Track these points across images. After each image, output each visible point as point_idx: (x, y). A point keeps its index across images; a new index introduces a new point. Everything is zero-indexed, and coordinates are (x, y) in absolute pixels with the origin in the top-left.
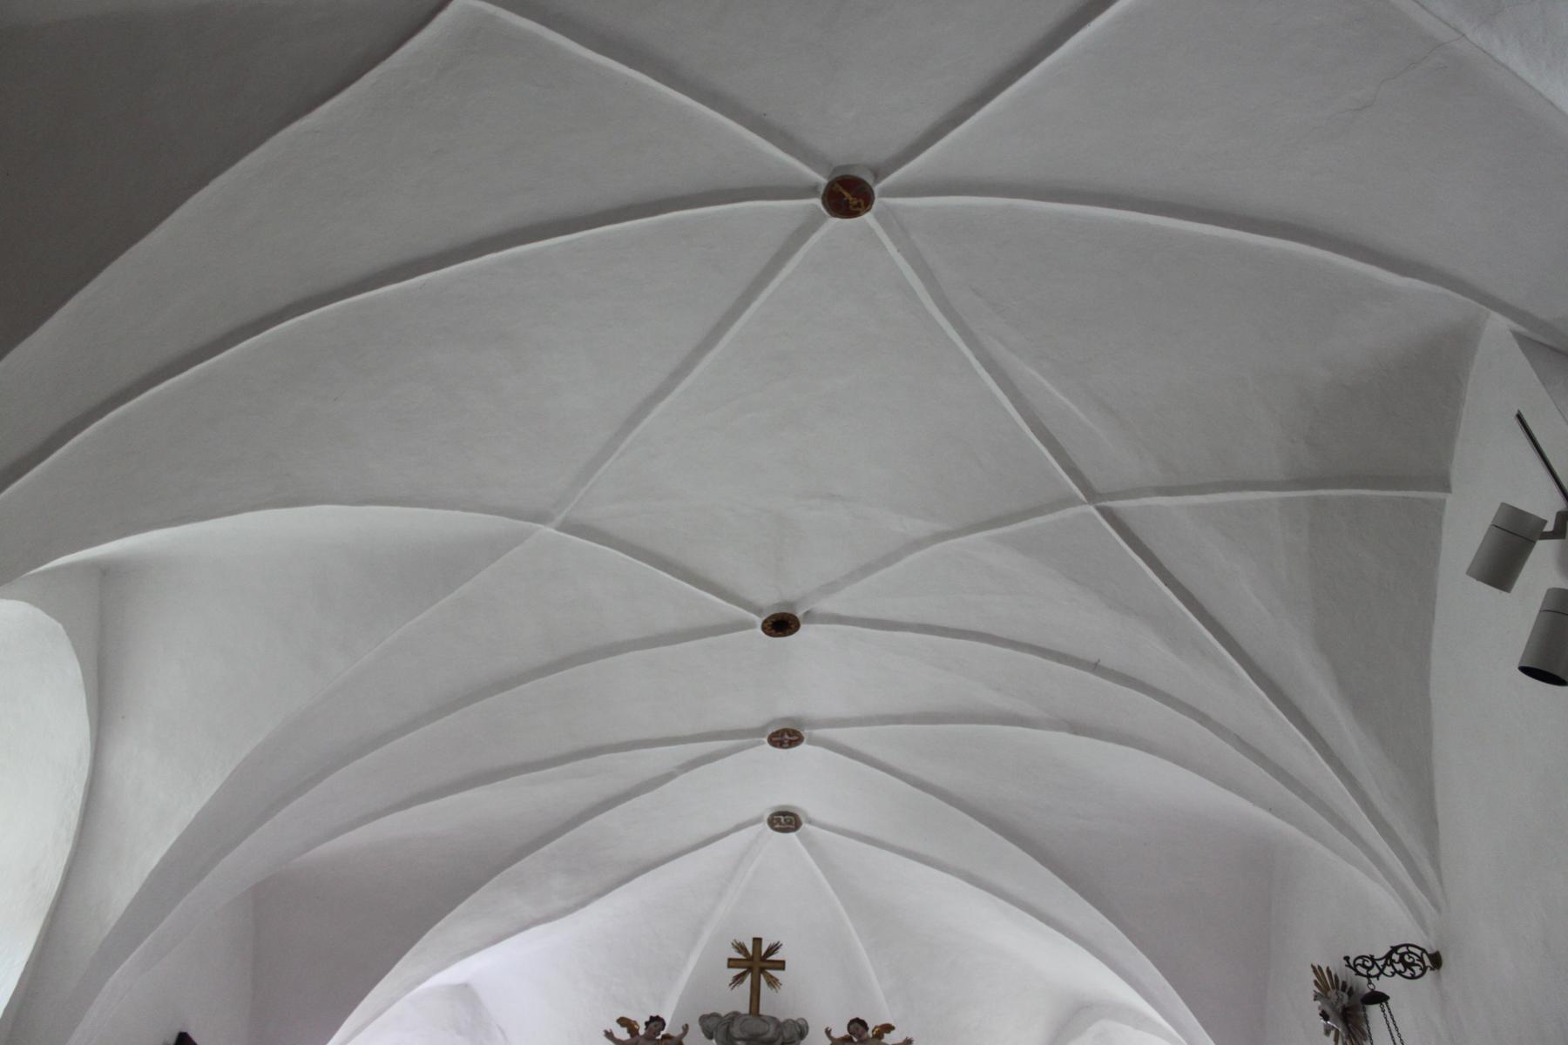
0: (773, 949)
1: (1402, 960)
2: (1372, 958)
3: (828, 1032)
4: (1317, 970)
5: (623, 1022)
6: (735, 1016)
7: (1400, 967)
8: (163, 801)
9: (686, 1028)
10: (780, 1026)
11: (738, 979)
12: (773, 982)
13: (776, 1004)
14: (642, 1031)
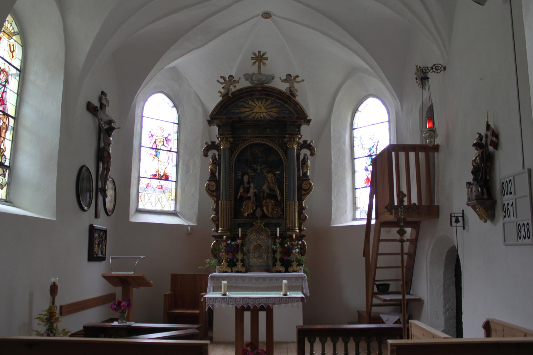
0: (264, 54)
1: (436, 68)
2: (428, 68)
3: (280, 78)
4: (417, 66)
5: (222, 77)
6: (254, 74)
7: (434, 70)
8: (86, 34)
9: (240, 78)
10: (267, 77)
11: (254, 63)
12: (264, 64)
14: (227, 79)
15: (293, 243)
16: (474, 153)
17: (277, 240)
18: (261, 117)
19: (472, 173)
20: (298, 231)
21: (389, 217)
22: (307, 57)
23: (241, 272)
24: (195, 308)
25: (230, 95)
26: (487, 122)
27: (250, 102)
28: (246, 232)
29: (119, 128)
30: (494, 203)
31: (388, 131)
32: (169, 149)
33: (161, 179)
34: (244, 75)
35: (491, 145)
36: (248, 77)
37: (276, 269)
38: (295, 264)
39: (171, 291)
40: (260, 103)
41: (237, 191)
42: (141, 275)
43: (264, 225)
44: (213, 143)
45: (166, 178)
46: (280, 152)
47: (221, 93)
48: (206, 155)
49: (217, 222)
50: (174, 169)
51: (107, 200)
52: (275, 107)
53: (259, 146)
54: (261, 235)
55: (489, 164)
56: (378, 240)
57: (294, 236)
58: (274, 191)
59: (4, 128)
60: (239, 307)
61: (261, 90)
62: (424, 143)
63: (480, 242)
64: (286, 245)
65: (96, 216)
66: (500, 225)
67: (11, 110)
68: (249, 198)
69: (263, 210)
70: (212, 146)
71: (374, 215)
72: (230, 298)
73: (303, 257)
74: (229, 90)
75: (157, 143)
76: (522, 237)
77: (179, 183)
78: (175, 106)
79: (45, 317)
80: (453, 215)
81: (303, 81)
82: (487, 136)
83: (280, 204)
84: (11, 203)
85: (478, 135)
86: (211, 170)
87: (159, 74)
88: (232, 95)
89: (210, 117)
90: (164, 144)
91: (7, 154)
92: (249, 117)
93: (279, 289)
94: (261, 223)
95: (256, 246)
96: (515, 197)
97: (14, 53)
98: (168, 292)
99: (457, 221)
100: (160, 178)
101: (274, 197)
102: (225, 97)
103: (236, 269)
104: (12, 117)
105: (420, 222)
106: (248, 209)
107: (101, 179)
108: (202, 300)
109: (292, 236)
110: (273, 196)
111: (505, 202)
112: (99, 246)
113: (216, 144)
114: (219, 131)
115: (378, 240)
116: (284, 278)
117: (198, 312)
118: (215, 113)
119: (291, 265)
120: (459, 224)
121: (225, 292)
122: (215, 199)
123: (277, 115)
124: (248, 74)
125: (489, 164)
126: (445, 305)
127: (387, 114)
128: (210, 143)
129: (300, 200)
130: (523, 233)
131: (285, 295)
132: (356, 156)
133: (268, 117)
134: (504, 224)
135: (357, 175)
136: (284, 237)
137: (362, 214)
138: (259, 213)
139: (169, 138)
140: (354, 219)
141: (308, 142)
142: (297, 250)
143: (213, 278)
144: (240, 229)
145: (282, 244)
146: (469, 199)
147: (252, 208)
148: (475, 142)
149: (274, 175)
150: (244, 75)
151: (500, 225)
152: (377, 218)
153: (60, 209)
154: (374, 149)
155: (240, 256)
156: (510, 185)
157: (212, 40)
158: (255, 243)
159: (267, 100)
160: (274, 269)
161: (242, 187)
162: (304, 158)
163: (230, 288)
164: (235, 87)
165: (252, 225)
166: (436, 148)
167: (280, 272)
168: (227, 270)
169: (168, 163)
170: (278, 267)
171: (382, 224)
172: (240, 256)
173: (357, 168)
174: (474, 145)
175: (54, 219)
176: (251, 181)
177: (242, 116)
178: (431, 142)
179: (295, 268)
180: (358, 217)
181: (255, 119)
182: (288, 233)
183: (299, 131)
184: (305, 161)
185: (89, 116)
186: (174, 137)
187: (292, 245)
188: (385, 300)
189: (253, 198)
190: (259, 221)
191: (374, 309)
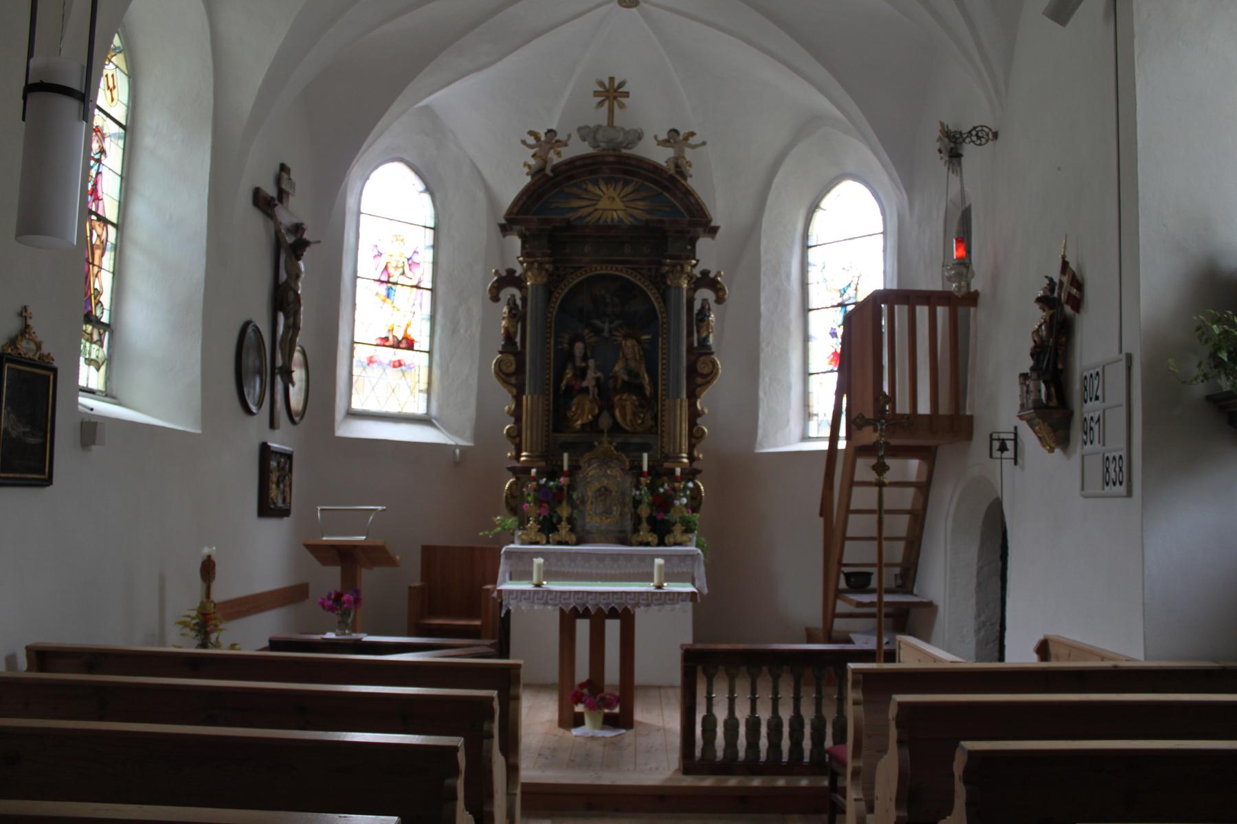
0: (622, 85)
2: (961, 133)
3: (656, 137)
4: (942, 124)
5: (531, 133)
6: (599, 127)
7: (974, 138)
8: (257, 48)
9: (569, 136)
10: (627, 133)
11: (600, 104)
12: (622, 106)
13: (622, 119)
14: (543, 138)
15: (676, 485)
16: (1037, 316)
17: (642, 479)
18: (613, 219)
19: (1032, 355)
20: (685, 460)
21: (869, 436)
22: (712, 93)
23: (566, 543)
24: (471, 616)
25: (548, 171)
26: (1064, 257)
27: (591, 188)
28: (577, 461)
29: (318, 242)
30: (1069, 416)
31: (881, 254)
32: (415, 283)
33: (398, 347)
34: (580, 129)
35: (1067, 303)
36: (586, 133)
37: (640, 539)
38: (678, 528)
39: (422, 580)
40: (611, 190)
41: (559, 376)
42: (379, 542)
43: (616, 448)
44: (511, 272)
45: (410, 345)
46: (653, 296)
47: (529, 167)
48: (495, 298)
49: (517, 440)
50: (426, 326)
51: (292, 390)
52: (641, 200)
53: (607, 283)
54: (609, 467)
55: (1063, 339)
56: (851, 483)
57: (678, 471)
58: (637, 375)
59: (98, 247)
60: (567, 610)
61: (613, 163)
62: (947, 289)
63: (1041, 487)
64: (661, 490)
65: (273, 424)
66: (1076, 458)
67: (110, 209)
68: (586, 390)
69: (613, 416)
70: (508, 279)
71: (843, 432)
72: (550, 592)
73: (697, 516)
74: (545, 162)
75: (391, 270)
76: (1111, 484)
77: (436, 357)
78: (428, 190)
79: (194, 621)
80: (995, 436)
81: (704, 143)
82: (1061, 283)
83: (650, 403)
84: (113, 397)
85: (1047, 281)
86: (507, 329)
87: (396, 125)
88: (552, 171)
89: (506, 219)
90: (403, 273)
91: (106, 299)
92: (588, 219)
93: (648, 577)
94: (611, 443)
95: (599, 490)
96: (1103, 405)
97: (115, 92)
98: (417, 583)
99: (1003, 448)
100: (397, 345)
101: (638, 389)
102: (539, 176)
103: (558, 538)
104: (112, 224)
105: (936, 447)
106: (582, 413)
107: (282, 349)
108: (495, 594)
109: (672, 471)
110: (633, 386)
111: (1086, 415)
112: (278, 486)
113: (517, 274)
114: (523, 247)
115: (851, 483)
116: (658, 556)
117: (478, 623)
118: (515, 210)
119: (670, 532)
120: (1006, 454)
121: (539, 579)
122: (514, 391)
123: (648, 217)
124: (586, 127)
125: (1063, 339)
126: (978, 616)
127: (881, 217)
128: (504, 274)
129: (692, 396)
130: (1113, 475)
131: (659, 587)
132: (813, 303)
133: (628, 221)
134: (1083, 457)
135: (813, 345)
136: (658, 472)
137: (820, 428)
138: (605, 422)
139: (416, 259)
140: (805, 438)
141: (712, 275)
142: (685, 501)
143: (510, 554)
144: (566, 456)
145: (652, 488)
146: (1022, 406)
147: (591, 412)
148: (1040, 293)
149: (639, 342)
150: (580, 129)
151: (1076, 458)
152: (848, 438)
153: (208, 412)
154: (851, 292)
155: (564, 511)
156: (1096, 383)
157: (511, 52)
158: (596, 485)
159: (626, 183)
160: (635, 538)
161: (570, 366)
162: (703, 308)
163: (549, 575)
164: (559, 154)
165: (591, 447)
166: (972, 299)
167: (648, 544)
168: (538, 539)
169: (412, 312)
170: (644, 534)
171: (857, 450)
172: (564, 511)
173: (813, 330)
174: (1039, 300)
175: (197, 430)
176: (589, 354)
177: (572, 216)
178: (959, 288)
179: (679, 538)
180: (813, 433)
181: (601, 222)
182: (667, 465)
183: (693, 250)
184: (703, 314)
185: (256, 217)
186: (426, 257)
187: (674, 490)
188: (860, 604)
189: (593, 391)
190: (605, 438)
191: (839, 624)
